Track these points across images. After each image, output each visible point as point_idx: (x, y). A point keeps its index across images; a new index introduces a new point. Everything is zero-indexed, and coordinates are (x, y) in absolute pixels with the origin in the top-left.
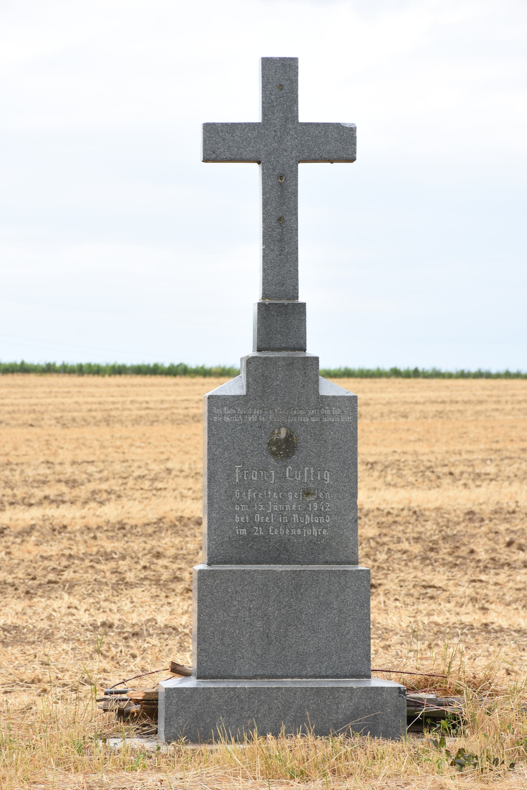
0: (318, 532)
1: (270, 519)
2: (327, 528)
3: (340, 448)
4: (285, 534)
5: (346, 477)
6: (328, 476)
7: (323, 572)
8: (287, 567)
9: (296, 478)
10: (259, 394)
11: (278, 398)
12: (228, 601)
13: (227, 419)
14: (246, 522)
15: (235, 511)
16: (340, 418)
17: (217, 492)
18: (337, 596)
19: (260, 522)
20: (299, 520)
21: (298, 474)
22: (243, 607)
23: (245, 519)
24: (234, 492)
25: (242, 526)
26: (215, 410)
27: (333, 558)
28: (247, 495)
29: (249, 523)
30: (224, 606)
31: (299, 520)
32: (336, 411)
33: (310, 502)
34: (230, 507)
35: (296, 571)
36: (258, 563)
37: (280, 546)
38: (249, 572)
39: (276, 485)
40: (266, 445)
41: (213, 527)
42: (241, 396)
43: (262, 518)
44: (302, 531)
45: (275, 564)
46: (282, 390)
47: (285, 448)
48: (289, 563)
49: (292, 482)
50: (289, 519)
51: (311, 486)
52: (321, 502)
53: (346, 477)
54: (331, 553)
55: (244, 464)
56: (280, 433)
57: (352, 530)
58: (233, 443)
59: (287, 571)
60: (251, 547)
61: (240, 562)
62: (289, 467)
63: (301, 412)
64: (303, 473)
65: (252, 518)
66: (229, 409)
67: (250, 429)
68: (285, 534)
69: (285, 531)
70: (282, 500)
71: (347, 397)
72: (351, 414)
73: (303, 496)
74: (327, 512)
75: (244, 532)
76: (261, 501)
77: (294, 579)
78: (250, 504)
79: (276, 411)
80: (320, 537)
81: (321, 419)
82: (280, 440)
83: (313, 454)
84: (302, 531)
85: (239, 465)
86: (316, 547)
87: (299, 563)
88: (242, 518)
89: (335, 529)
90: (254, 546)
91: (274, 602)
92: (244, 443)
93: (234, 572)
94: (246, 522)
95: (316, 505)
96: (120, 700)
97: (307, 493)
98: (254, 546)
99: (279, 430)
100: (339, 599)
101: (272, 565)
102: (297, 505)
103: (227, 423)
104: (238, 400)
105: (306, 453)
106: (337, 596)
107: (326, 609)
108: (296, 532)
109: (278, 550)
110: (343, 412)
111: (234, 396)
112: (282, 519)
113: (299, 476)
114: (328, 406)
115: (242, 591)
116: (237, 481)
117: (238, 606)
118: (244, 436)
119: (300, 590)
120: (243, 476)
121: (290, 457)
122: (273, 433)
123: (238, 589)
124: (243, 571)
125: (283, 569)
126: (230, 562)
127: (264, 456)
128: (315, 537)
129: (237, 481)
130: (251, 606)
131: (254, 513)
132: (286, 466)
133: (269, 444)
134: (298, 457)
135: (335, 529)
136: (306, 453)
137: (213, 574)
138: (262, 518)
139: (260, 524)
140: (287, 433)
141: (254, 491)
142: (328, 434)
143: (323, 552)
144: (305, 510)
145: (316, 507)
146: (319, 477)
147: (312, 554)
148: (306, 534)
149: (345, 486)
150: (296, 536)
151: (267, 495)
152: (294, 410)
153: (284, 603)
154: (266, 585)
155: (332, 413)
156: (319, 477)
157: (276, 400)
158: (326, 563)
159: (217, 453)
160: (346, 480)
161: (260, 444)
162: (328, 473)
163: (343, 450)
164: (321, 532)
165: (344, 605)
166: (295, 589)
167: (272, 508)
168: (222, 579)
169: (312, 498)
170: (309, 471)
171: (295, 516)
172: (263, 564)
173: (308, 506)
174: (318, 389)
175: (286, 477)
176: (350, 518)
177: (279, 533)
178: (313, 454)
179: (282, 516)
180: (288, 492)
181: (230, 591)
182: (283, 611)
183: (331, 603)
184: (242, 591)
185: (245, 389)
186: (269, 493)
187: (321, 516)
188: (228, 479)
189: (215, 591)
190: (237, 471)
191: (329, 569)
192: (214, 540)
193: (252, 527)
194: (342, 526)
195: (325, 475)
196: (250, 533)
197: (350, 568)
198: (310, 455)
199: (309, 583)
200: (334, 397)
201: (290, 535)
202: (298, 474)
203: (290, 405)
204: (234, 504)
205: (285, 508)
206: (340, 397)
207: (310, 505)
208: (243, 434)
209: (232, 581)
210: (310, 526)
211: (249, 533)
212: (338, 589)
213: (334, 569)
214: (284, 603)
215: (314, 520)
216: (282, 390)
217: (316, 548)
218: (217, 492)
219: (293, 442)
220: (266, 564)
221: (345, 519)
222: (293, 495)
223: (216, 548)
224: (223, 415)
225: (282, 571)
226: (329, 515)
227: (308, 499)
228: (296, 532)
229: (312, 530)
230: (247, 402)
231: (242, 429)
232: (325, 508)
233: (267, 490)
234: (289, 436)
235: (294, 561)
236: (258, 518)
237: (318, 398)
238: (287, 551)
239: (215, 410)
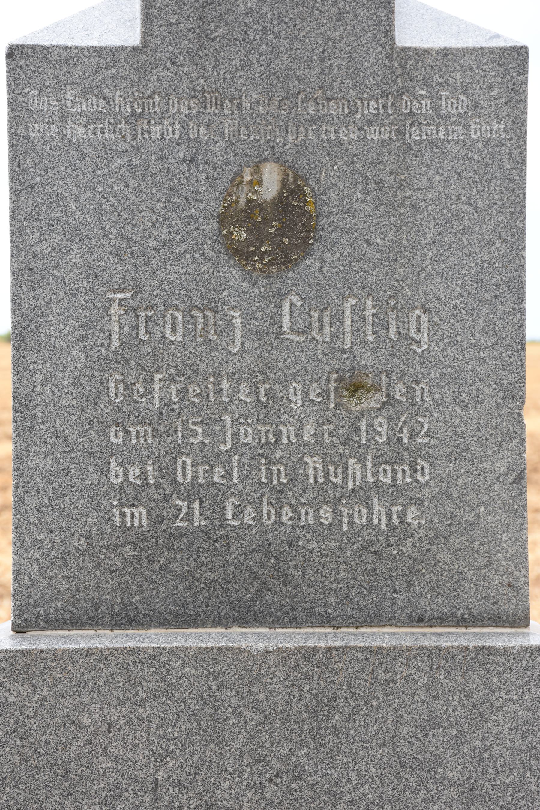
0: (389, 514)
1: (229, 474)
2: (420, 504)
3: (464, 232)
4: (279, 522)
5: (484, 331)
6: (425, 326)
7: (408, 655)
8: (287, 637)
9: (314, 333)
10: (187, 44)
11: (254, 58)
12: (79, 757)
13: (77, 132)
14: (145, 484)
15: (109, 446)
16: (467, 127)
17: (45, 382)
18: (460, 739)
19: (194, 484)
20: (327, 475)
21: (321, 320)
22: (134, 780)
23: (144, 473)
24: (104, 383)
25: (131, 495)
26: (33, 98)
27: (442, 605)
28: (148, 392)
29: (158, 485)
30: (65, 777)
31: (327, 475)
32: (453, 104)
33: (362, 414)
34: (92, 435)
35: (315, 650)
36: (186, 622)
37: (262, 563)
38: (153, 656)
39: (248, 358)
40: (214, 225)
41: (32, 501)
42: (123, 49)
43: (201, 469)
44: (337, 513)
45: (246, 624)
46: (265, 31)
47: (276, 232)
48: (294, 622)
49: (301, 347)
50: (292, 472)
51: (368, 360)
52: (399, 414)
53: (484, 331)
54: (435, 588)
55: (137, 288)
56: (260, 182)
57: (506, 507)
58: (99, 214)
59: (285, 650)
60: (164, 568)
61: (127, 620)
62: (293, 298)
63: (333, 109)
64: (338, 318)
65: (167, 471)
66: (85, 94)
67: (156, 167)
68: (279, 522)
69: (279, 514)
70: (269, 409)
71: (492, 51)
72: (505, 111)
73: (339, 396)
74: (420, 447)
75: (139, 516)
76: (199, 413)
77: (307, 677)
78: (160, 422)
79: (246, 104)
80: (398, 532)
81: (401, 133)
82: (261, 206)
83: (371, 253)
84: (337, 513)
85: (120, 290)
86: (383, 568)
87: (327, 621)
88: (134, 472)
89: (449, 506)
90: (176, 567)
91: (240, 758)
92: (138, 217)
93: (102, 656)
94: (145, 484)
95: (382, 425)
96: (291, 315)
97: (354, 386)
98: (176, 567)
99: (257, 170)
100: (465, 749)
101: (236, 630)
102: (319, 425)
103: (78, 147)
104: (115, 63)
105: (347, 250)
106: (460, 739)
107: (420, 783)
108: (317, 517)
109: (255, 576)
110: (476, 106)
111: (99, 51)
112: (269, 472)
113: (327, 329)
114: (425, 85)
115: (129, 723)
116: (116, 343)
117: (113, 778)
118: (137, 191)
119: (328, 717)
120: (135, 328)
121: (296, 263)
122: (236, 181)
123: (117, 715)
124: (132, 652)
125: (271, 645)
126: (92, 621)
127: (207, 259)
128: (379, 531)
129: (116, 343)
130: (160, 776)
131: (175, 453)
132: (281, 295)
133: (222, 219)
134: (323, 262)
135: (449, 506)
136: (347, 250)
137: (28, 667)
138: (201, 469)
139: (193, 492)
140: (284, 182)
141: (172, 380)
142: (423, 183)
143: (410, 584)
144: (346, 442)
145: (384, 431)
146: (393, 330)
147: (372, 589)
148: (351, 523)
149: (482, 361)
150: (318, 531)
151: (219, 391)
152: (306, 99)
153: (276, 764)
154: (211, 700)
155: (437, 109)
156: (393, 330)
157: (245, 65)
158: (420, 620)
159: (44, 248)
160: (488, 340)
161: (190, 220)
162: (425, 318)
163: (474, 238)
164: (402, 516)
165: (485, 772)
166: (314, 715)
167: (236, 436)
168: (57, 682)
169: (370, 402)
170: (359, 312)
171: (314, 462)
172: (203, 625)
173: (357, 430)
174: (391, 24)
175: (279, 334)
176: (501, 467)
177: (258, 519)
178: (371, 253)
179: (269, 462)
180: (288, 381)
181: (86, 722)
182: (270, 790)
183: (439, 761)
184: (129, 723)
185: (138, 29)
186: (225, 385)
187: (401, 460)
188: (82, 339)
189: (33, 724)
190: (114, 309)
191: (428, 643)
192: (38, 545)
193: (166, 499)
194: (471, 497)
195: (413, 325)
196: (160, 519)
197: (501, 638)
198: (362, 257)
199: (360, 692)
200: (445, 53)
201: (294, 527)
202: (321, 320)
203: (294, 85)
204: (103, 426)
205: (278, 435)
206: (465, 51)
207: (363, 424)
208: (133, 183)
209: (95, 689)
210: (363, 494)
211: (156, 520)
212: (460, 711)
213: (444, 643)
214: (276, 764)
215: (375, 474)
216: (265, 31)
217: (383, 568)
218: (45, 382)
219: (304, 213)
220: (217, 623)
221: (481, 473)
222: (306, 393)
223: (42, 572)
224: (63, 118)
225: (267, 652)
226: (428, 457)
227: (355, 406)
228: (317, 517)
229: (370, 508)
230: (145, 71)
231: (130, 167)
232: (413, 436)
233: (218, 375)
234: (292, 192)
235: (310, 612)
236: (187, 470)
237: (390, 58)
238: (286, 579)
239: (33, 98)
